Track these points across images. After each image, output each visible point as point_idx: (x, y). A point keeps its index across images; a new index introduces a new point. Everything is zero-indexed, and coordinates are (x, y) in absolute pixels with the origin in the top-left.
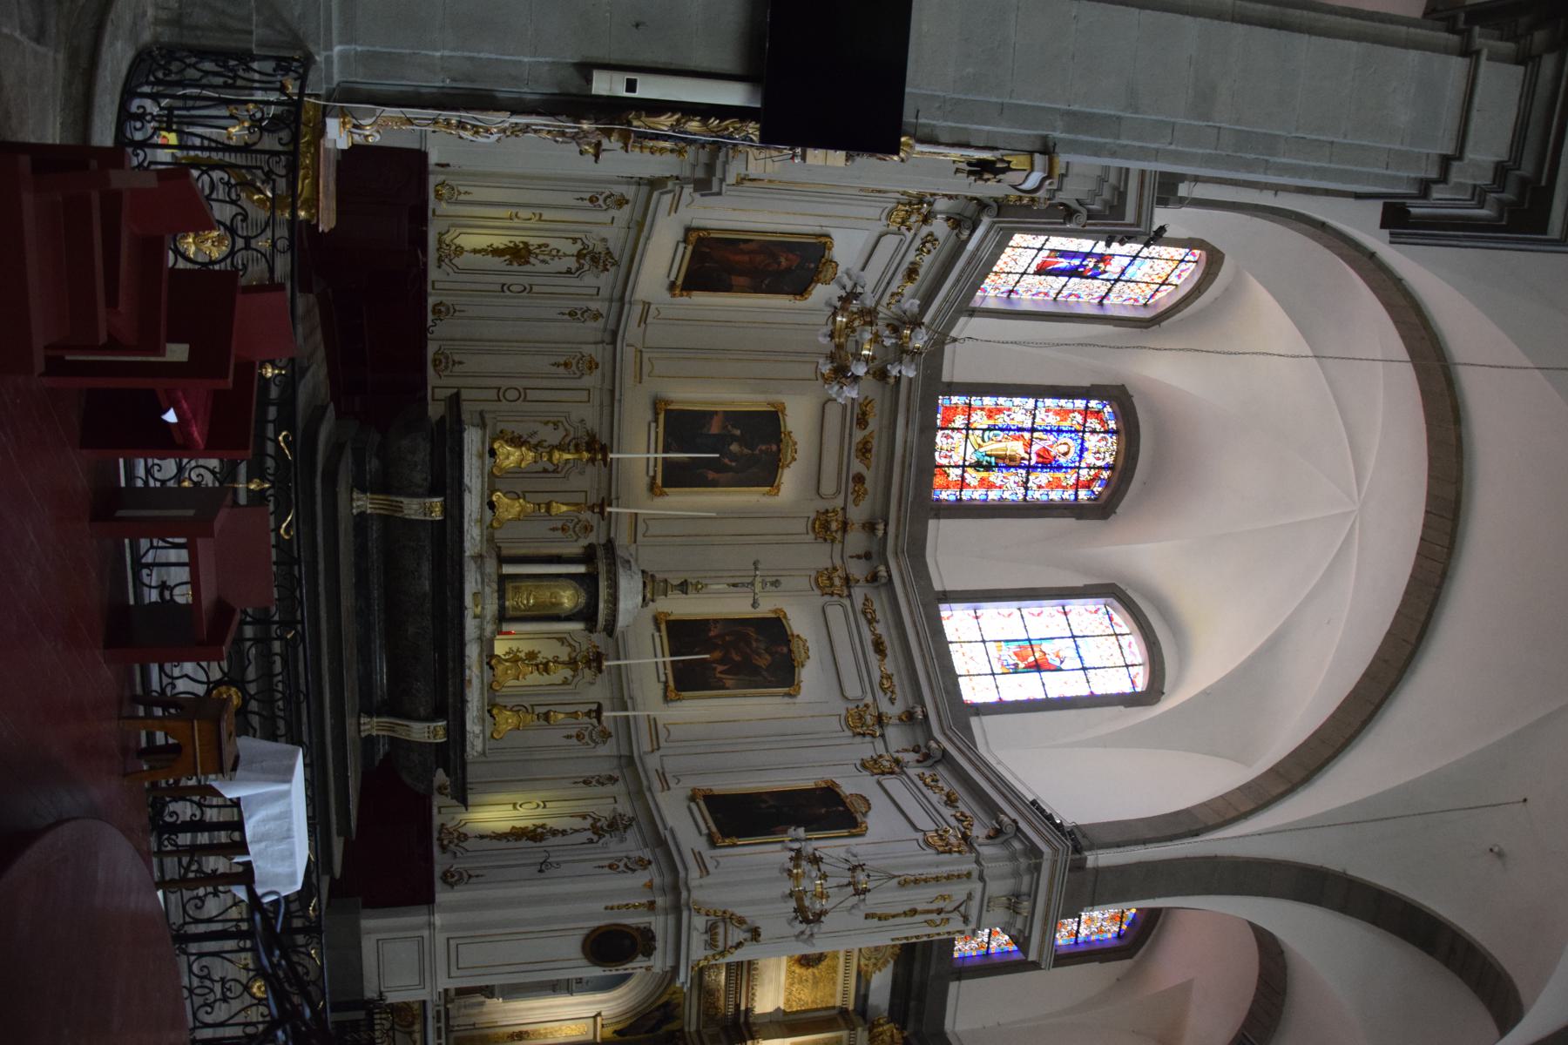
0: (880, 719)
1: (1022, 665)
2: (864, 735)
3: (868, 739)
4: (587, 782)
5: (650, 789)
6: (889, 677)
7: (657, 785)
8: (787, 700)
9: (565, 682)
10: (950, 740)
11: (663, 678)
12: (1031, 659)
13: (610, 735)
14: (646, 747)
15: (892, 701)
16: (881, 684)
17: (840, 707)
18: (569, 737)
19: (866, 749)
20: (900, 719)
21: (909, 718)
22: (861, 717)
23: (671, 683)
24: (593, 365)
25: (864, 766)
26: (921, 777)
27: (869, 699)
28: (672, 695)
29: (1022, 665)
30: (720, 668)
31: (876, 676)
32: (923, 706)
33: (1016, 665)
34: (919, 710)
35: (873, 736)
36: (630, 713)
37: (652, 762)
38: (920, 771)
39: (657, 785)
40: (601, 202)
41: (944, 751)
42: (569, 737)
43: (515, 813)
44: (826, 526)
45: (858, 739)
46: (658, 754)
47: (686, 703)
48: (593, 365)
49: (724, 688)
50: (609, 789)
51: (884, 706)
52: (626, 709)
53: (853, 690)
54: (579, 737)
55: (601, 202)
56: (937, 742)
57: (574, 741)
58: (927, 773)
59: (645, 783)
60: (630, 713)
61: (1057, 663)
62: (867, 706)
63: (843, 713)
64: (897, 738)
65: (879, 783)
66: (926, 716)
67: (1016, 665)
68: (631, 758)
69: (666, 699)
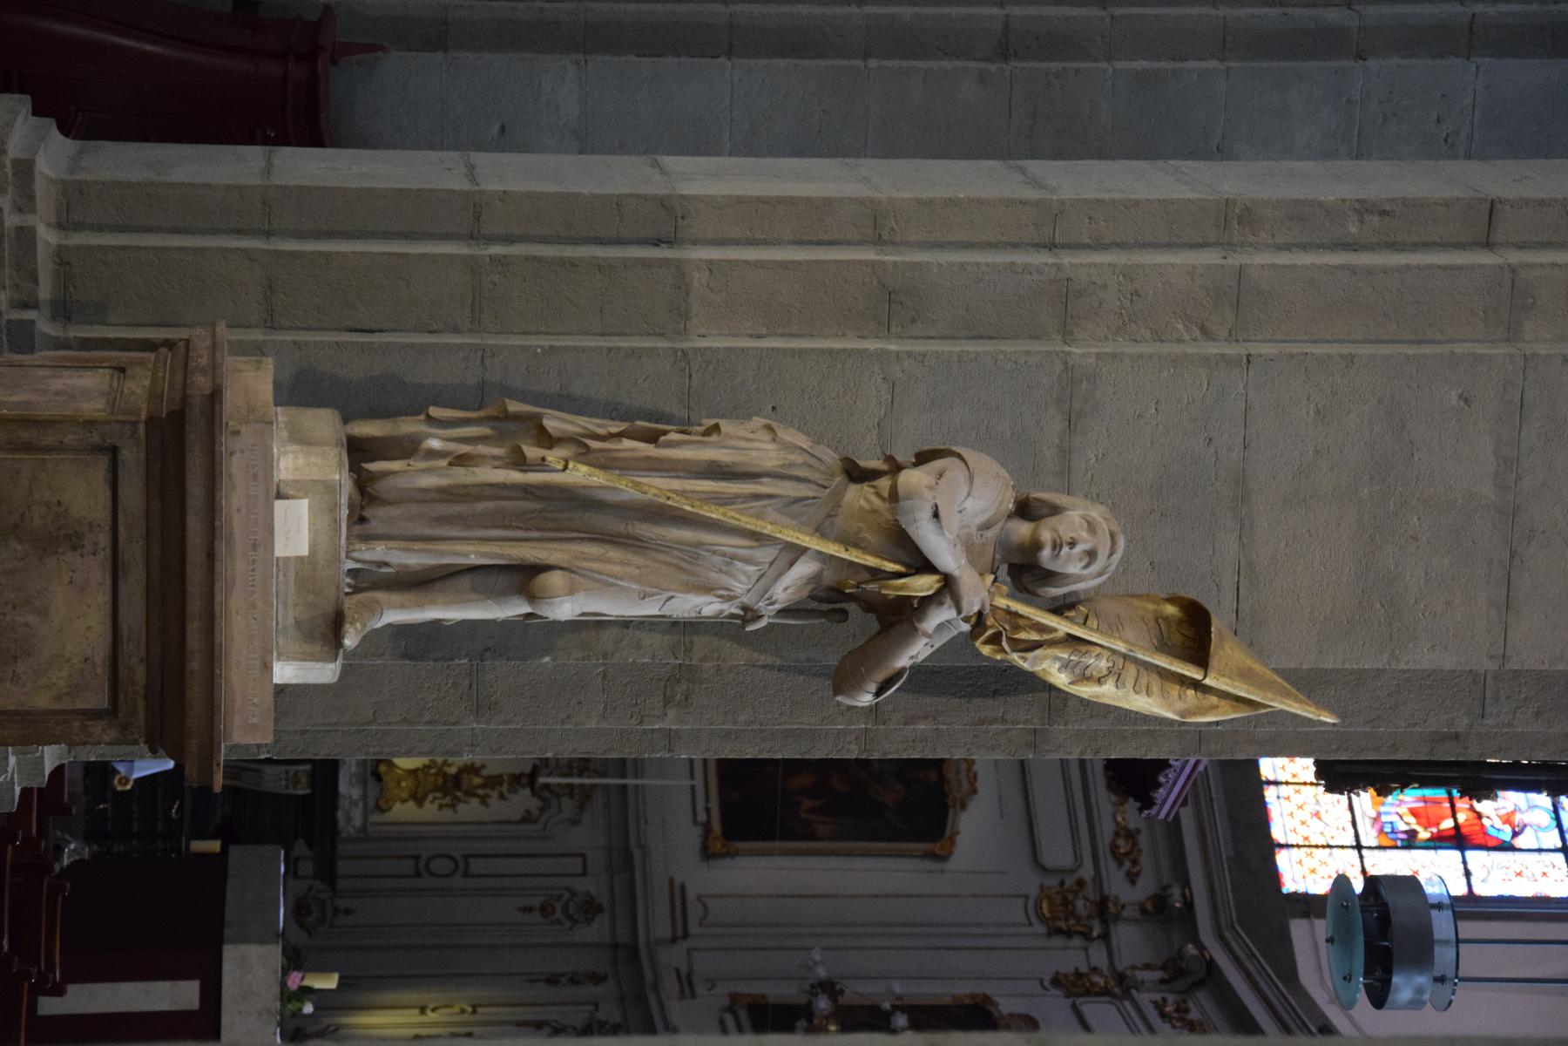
0: (1104, 909)
1: (1424, 834)
2: (1068, 934)
3: (1076, 942)
4: (552, 980)
5: (656, 988)
6: (1131, 835)
7: (670, 985)
8: (928, 864)
9: (527, 818)
10: (1227, 946)
11: (702, 817)
12: (1448, 824)
13: (600, 910)
14: (662, 929)
15: (1132, 878)
16: (1114, 848)
17: (1031, 883)
18: (527, 910)
19: (1071, 957)
20: (1143, 910)
21: (1159, 910)
22: (1066, 903)
23: (716, 826)
24: (591, 909)
25: (1057, 981)
26: (1159, 1007)
27: (1087, 872)
28: (717, 846)
29: (1424, 834)
30: (808, 803)
31: (1106, 830)
32: (1185, 883)
33: (1412, 834)
34: (1176, 891)
35: (1087, 936)
36: (630, 781)
37: (671, 957)
38: (1157, 997)
39: (670, 985)
40: (558, 914)
41: (1211, 965)
42: (527, 910)
43: (423, 1019)
44: (1466, 400)
45: (1057, 941)
46: (684, 945)
47: (741, 862)
48: (591, 909)
49: (812, 837)
50: (588, 990)
51: (1117, 885)
52: (624, 776)
53: (1058, 853)
54: (545, 910)
55: (558, 914)
56: (1200, 947)
57: (537, 917)
58: (1171, 998)
59: (648, 976)
60: (630, 781)
61: (1506, 834)
62: (1081, 883)
63: (1034, 892)
64: (1132, 944)
65: (1075, 1009)
66: (1189, 905)
67: (1412, 834)
68: (633, 950)
69: (707, 854)
